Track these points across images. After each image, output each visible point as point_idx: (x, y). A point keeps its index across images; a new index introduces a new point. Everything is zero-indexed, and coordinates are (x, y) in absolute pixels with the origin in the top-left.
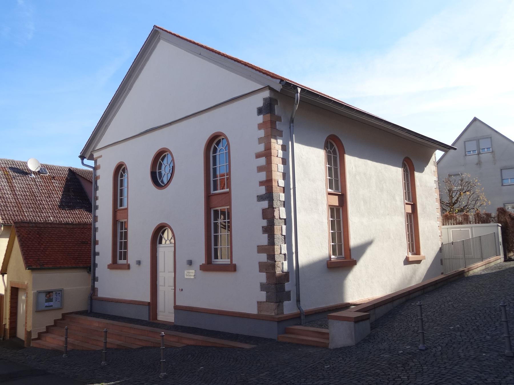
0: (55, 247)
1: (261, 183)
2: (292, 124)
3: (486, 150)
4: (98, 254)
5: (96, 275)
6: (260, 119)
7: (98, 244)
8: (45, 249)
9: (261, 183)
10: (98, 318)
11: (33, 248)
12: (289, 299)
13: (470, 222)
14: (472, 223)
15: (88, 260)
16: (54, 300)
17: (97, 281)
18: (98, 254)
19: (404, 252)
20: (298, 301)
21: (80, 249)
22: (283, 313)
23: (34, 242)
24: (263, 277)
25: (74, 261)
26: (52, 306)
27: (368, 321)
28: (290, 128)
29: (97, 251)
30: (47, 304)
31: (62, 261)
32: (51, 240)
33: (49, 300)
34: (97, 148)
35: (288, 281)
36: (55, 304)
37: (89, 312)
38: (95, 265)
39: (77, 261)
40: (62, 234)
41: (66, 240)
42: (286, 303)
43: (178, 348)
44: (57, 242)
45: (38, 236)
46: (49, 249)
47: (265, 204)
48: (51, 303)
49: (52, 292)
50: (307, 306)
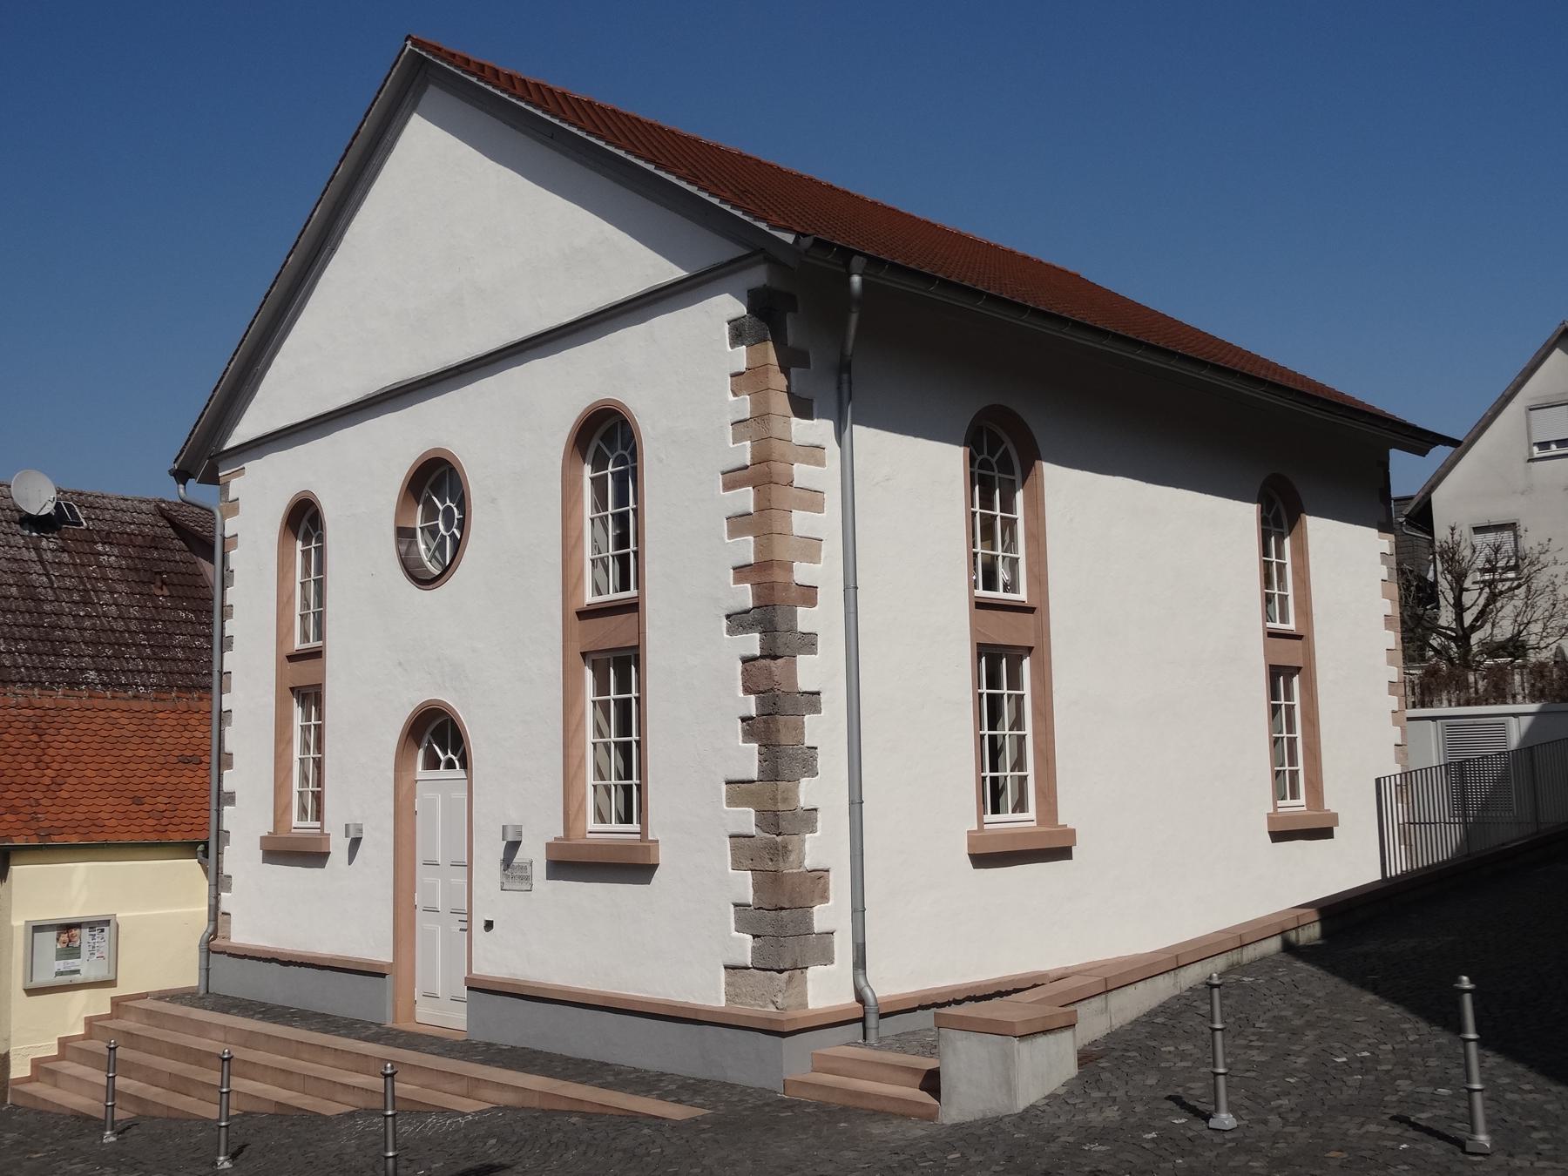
0: (88, 773)
1: (741, 572)
2: (845, 376)
3: (1554, 447)
4: (231, 798)
5: (226, 871)
6: (740, 357)
7: (230, 766)
8: (59, 780)
9: (741, 572)
10: (252, 1017)
11: (18, 780)
12: (827, 957)
13: (1514, 696)
14: (1519, 698)
15: (200, 821)
16: (85, 950)
17: (229, 890)
18: (231, 798)
19: (1257, 800)
20: (860, 963)
21: (174, 780)
22: (806, 1006)
23: (20, 758)
24: (744, 886)
25: (151, 822)
26: (77, 972)
27: (1068, 1034)
28: (839, 388)
29: (227, 786)
30: (61, 965)
31: (113, 822)
32: (77, 752)
33: (70, 951)
34: (231, 443)
35: (824, 898)
36: (88, 968)
37: (202, 992)
38: (222, 836)
39: (164, 822)
40: (116, 733)
41: (129, 753)
42: (813, 972)
43: (463, 1115)
44: (114, 752)
45: (34, 738)
46: (71, 780)
47: (752, 643)
48: (73, 964)
49: (78, 926)
50: (887, 984)
